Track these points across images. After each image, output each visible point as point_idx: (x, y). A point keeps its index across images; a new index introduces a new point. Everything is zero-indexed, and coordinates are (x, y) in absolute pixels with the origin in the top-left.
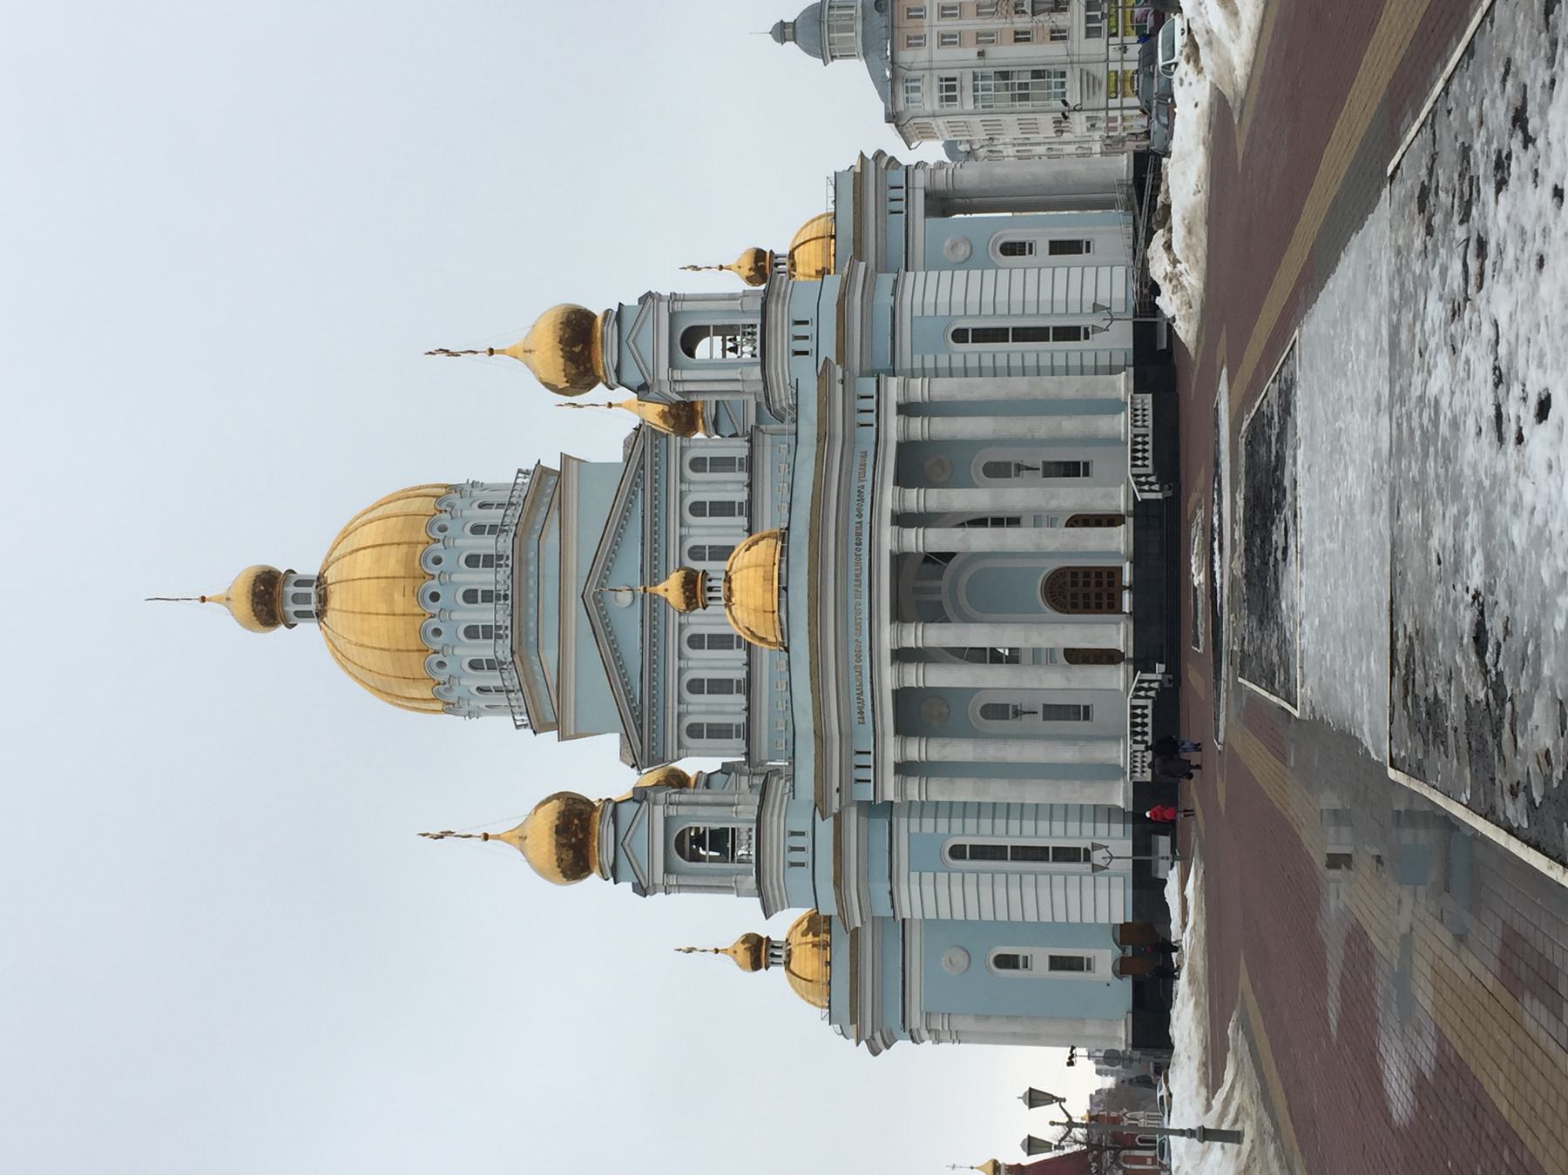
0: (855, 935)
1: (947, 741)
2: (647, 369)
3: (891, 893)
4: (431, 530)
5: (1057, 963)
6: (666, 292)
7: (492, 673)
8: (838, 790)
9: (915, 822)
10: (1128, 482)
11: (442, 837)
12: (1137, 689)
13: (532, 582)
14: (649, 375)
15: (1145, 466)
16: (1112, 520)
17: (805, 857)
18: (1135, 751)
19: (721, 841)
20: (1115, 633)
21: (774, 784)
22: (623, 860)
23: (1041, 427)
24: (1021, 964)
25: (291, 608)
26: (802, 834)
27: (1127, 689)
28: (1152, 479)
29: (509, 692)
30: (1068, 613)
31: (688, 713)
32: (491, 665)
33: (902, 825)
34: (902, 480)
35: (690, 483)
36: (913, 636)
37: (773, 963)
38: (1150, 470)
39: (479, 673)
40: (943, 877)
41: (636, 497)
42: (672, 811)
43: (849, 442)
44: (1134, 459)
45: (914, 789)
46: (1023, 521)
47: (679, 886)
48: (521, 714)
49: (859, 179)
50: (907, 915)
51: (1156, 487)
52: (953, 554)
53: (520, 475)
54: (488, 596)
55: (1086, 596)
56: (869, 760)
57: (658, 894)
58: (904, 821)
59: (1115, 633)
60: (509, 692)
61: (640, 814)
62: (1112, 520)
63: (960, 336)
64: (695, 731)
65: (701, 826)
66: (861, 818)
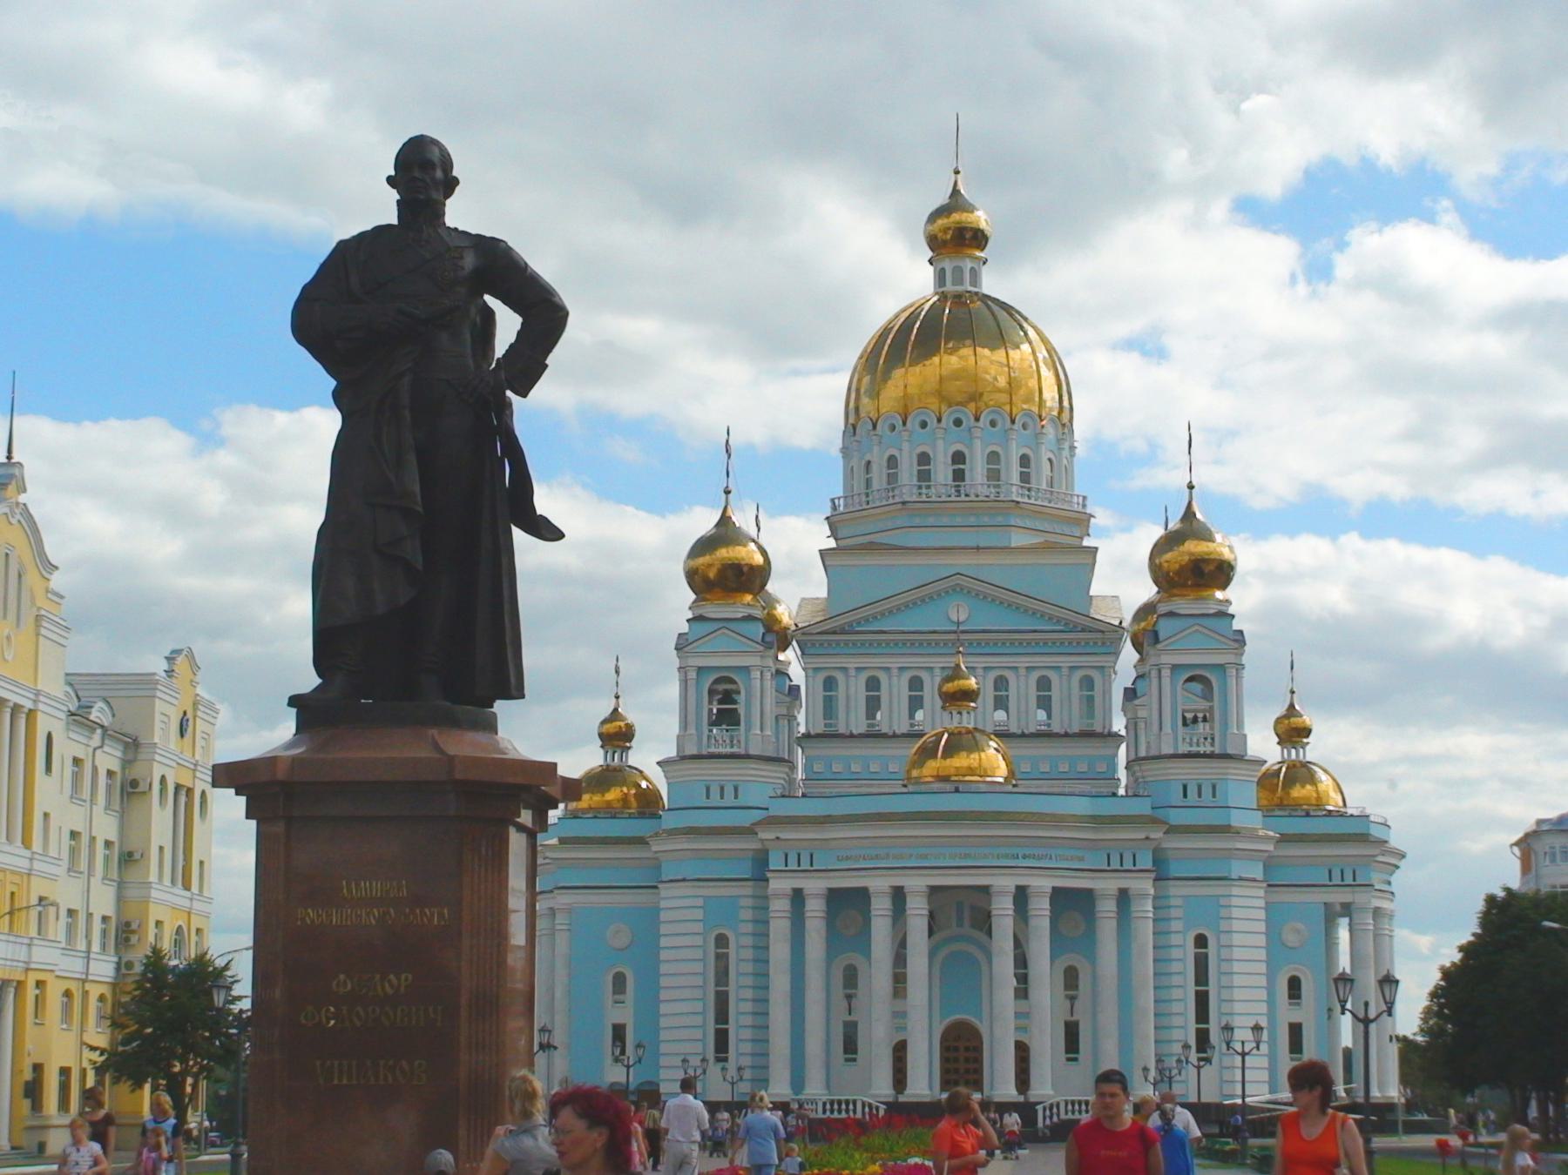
0: (641, 841)
1: (824, 934)
2: (1175, 642)
3: (684, 880)
4: (1025, 414)
5: (619, 1032)
6: (1245, 660)
7: (885, 478)
8: (778, 838)
9: (749, 902)
10: (1054, 1097)
11: (727, 451)
12: (870, 1105)
13: (972, 520)
14: (1167, 645)
15: (1066, 1113)
16: (1023, 1081)
17: (715, 800)
18: (816, 1104)
19: (727, 717)
20: (923, 1085)
21: (782, 769)
22: (709, 627)
23: (1109, 1016)
24: (618, 997)
25: (948, 265)
26: (736, 797)
27: (873, 1096)
28: (1055, 1119)
29: (867, 495)
30: (941, 1043)
31: (847, 676)
32: (892, 478)
33: (748, 889)
34: (1058, 894)
35: (1069, 676)
36: (917, 907)
37: (607, 752)
38: (1063, 1116)
39: (885, 464)
40: (699, 927)
41: (1055, 624)
42: (756, 674)
43: (1093, 845)
44: (1073, 1103)
45: (780, 906)
46: (1022, 1002)
47: (686, 681)
48: (845, 506)
49: (1363, 838)
50: (663, 893)
51: (1048, 1122)
52: (991, 937)
53: (1081, 498)
54: (959, 476)
55: (956, 1060)
56: (805, 865)
57: (678, 660)
58: (749, 891)
59: (923, 1085)
60: (867, 495)
61: (750, 643)
62: (1023, 1081)
63: (1201, 941)
64: (830, 684)
65: (742, 698)
66: (751, 853)
